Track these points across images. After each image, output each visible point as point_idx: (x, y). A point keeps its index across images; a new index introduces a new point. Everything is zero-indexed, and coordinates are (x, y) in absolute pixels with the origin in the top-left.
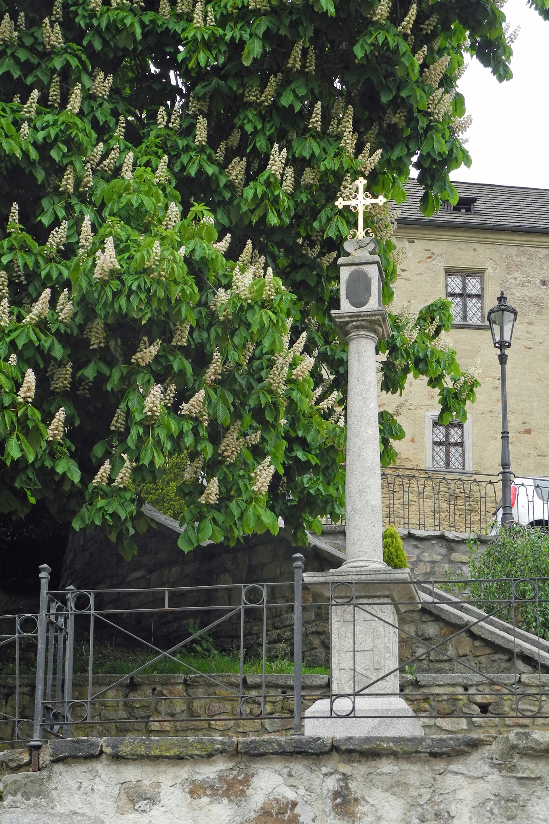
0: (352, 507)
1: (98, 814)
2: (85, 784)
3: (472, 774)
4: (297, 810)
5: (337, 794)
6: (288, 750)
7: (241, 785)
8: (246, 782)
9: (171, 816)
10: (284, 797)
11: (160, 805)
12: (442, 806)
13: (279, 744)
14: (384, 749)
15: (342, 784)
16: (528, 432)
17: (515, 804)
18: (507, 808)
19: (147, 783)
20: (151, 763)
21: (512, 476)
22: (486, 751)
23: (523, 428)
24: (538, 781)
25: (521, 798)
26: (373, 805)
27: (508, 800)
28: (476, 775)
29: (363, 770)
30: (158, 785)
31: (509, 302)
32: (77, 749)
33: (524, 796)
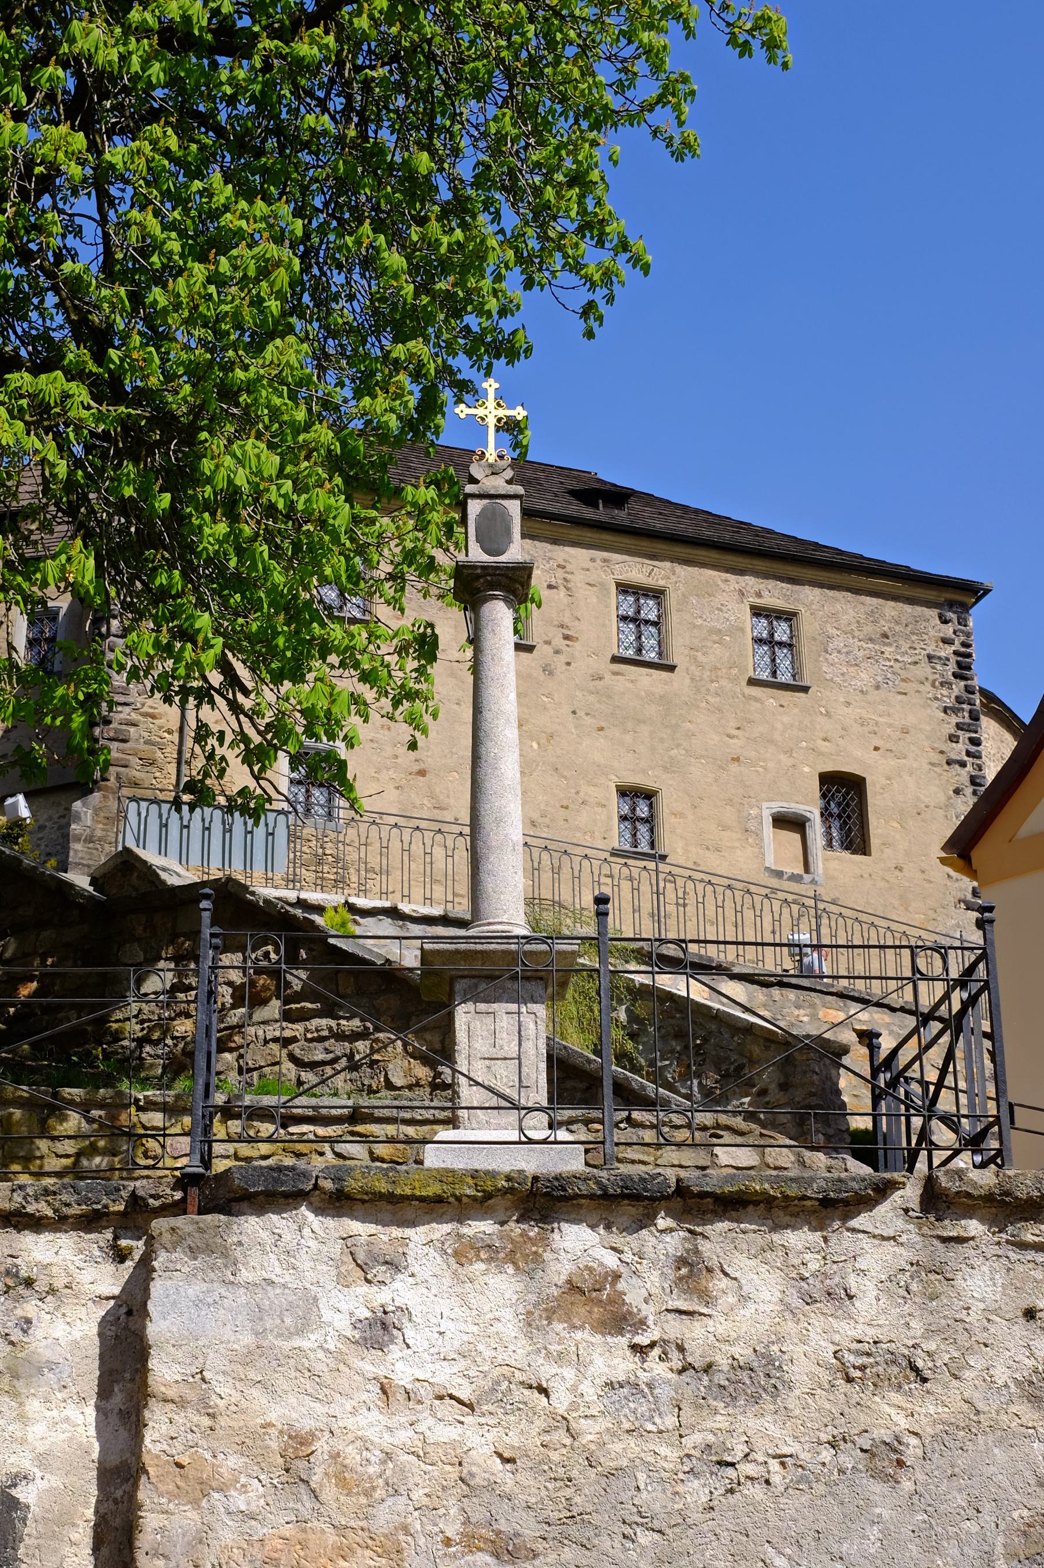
1: (308, 1286)
4: (621, 1285)
5: (681, 1261)
7: (534, 1245)
13: (598, 1183)
16: (422, 773)
23: (416, 768)
32: (276, 1181)
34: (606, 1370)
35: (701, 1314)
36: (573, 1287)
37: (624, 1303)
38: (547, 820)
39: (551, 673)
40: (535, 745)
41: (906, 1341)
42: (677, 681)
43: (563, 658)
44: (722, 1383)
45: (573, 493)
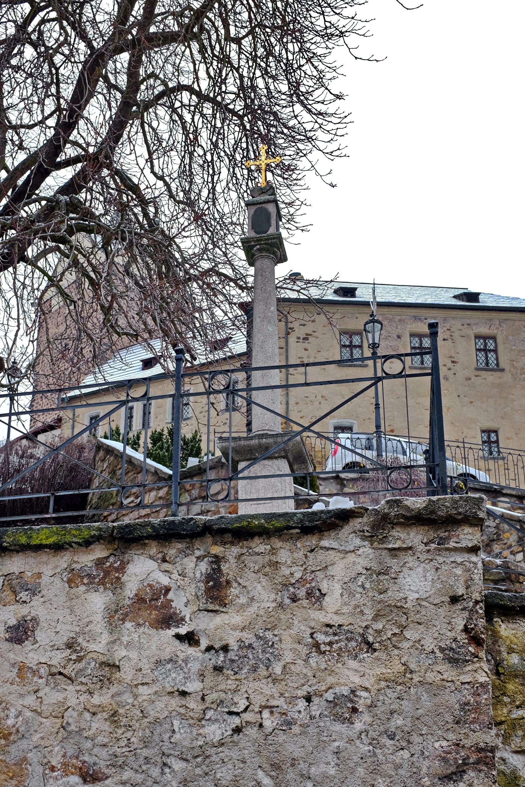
3: (343, 548)
4: (170, 596)
8: (122, 569)
9: (50, 606)
10: (157, 583)
11: (40, 595)
12: (313, 584)
13: (153, 527)
14: (256, 527)
17: (387, 577)
18: (379, 582)
19: (29, 574)
20: (33, 554)
22: (356, 523)
24: (410, 552)
25: (393, 571)
26: (244, 587)
27: (379, 574)
28: (347, 549)
29: (236, 551)
30: (39, 575)
33: (396, 568)
34: (158, 652)
35: (222, 612)
36: (139, 599)
37: (171, 607)
41: (360, 623)
42: (507, 377)
43: (452, 372)
44: (233, 658)
45: (455, 297)
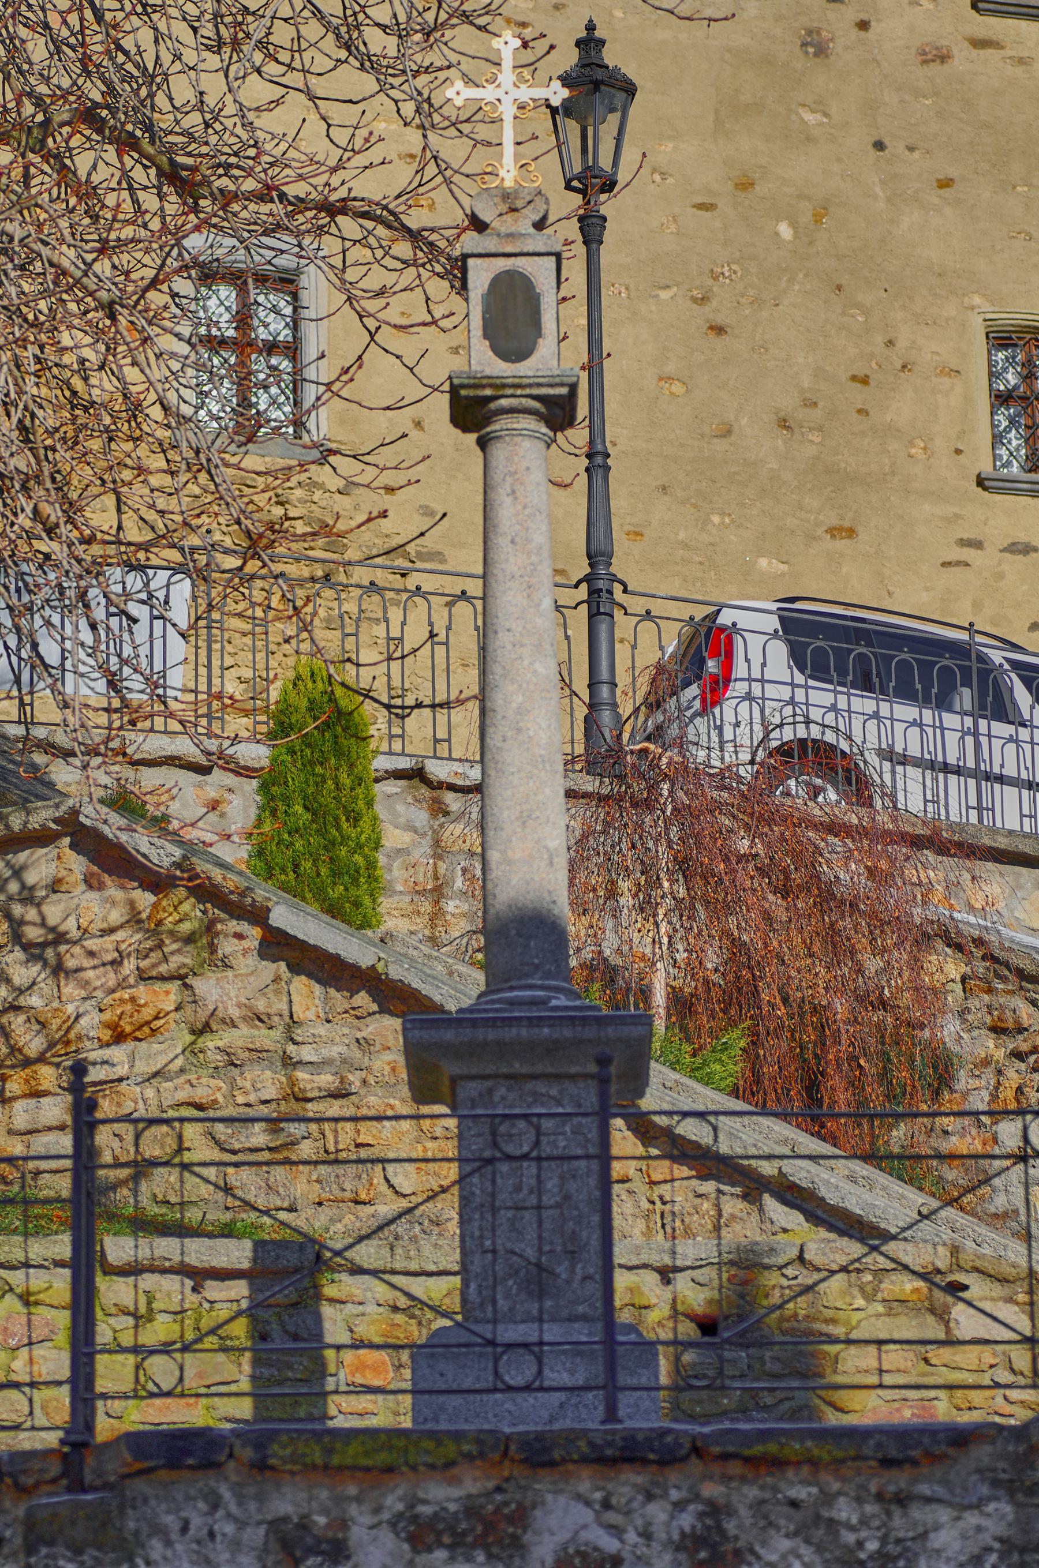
0: (503, 852)
2: (196, 1521)
3: (958, 1500)
6: (609, 1452)
8: (521, 1517)
10: (596, 1549)
15: (709, 1522)
21: (617, 588)
31: (610, 57)
38: (817, 414)
39: (821, 51)
40: (785, 231)
